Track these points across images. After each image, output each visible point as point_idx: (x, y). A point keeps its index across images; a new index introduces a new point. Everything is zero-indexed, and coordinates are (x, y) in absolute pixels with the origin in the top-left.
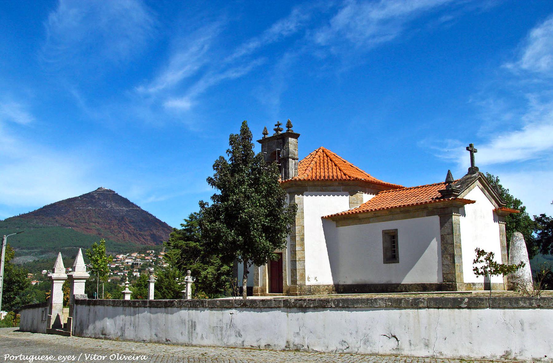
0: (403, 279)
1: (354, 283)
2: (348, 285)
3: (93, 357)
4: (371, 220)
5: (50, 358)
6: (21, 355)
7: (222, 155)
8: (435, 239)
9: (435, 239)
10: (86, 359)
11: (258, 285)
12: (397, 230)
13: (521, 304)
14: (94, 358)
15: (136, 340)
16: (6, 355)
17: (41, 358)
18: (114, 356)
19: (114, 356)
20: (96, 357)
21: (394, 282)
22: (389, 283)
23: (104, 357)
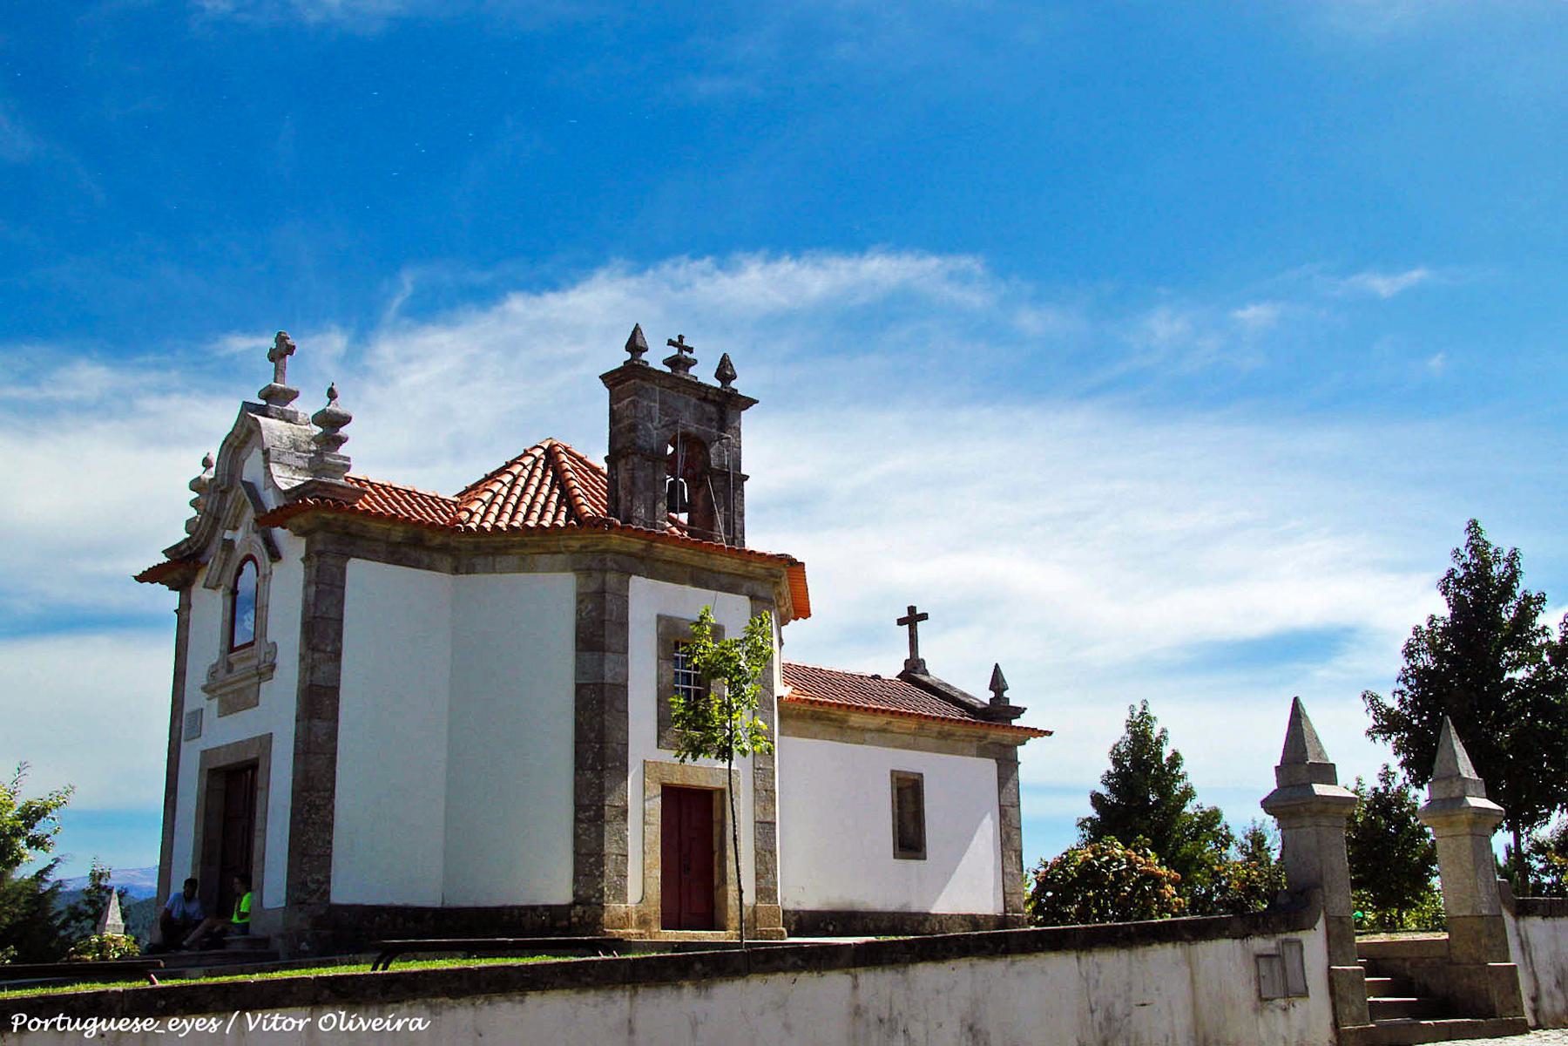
0: (934, 901)
1: (826, 908)
2: (811, 912)
3: (270, 1022)
4: (868, 736)
5: (144, 1024)
6: (61, 1017)
7: (1386, 761)
8: (989, 816)
9: (989, 816)
10: (251, 1028)
11: (621, 894)
12: (893, 772)
13: (790, 960)
14: (274, 1025)
15: (1186, 970)
16: (16, 1017)
17: (120, 1025)
18: (330, 1019)
19: (330, 1019)
20: (279, 1023)
21: (915, 908)
22: (906, 910)
23: (302, 1023)
